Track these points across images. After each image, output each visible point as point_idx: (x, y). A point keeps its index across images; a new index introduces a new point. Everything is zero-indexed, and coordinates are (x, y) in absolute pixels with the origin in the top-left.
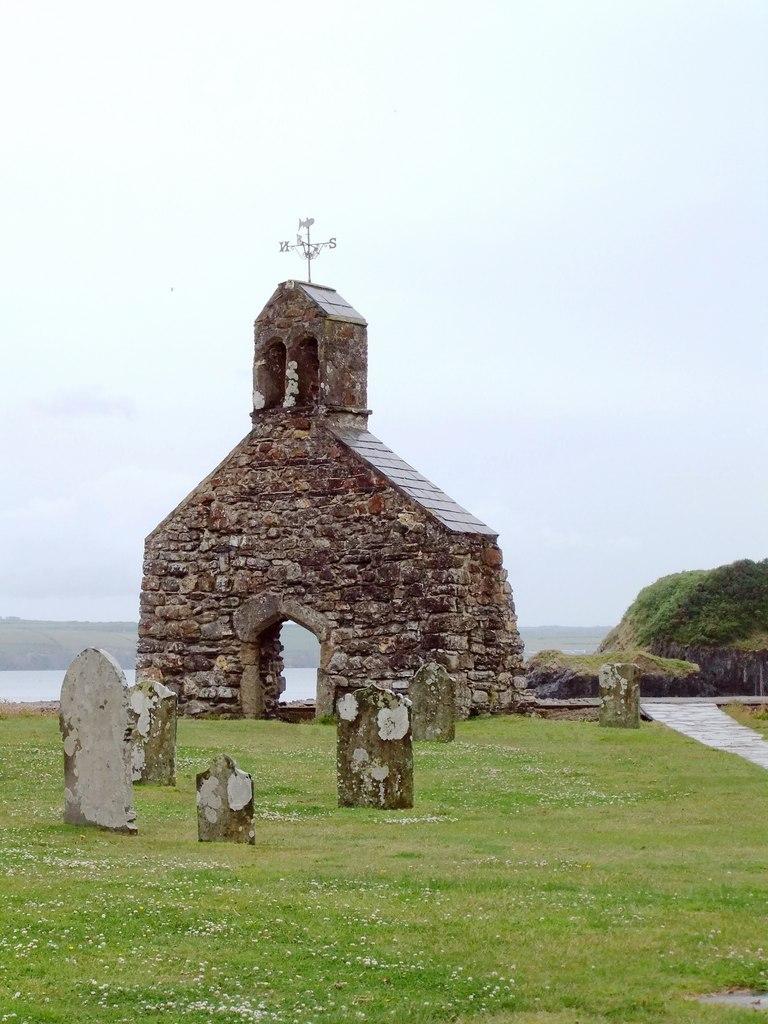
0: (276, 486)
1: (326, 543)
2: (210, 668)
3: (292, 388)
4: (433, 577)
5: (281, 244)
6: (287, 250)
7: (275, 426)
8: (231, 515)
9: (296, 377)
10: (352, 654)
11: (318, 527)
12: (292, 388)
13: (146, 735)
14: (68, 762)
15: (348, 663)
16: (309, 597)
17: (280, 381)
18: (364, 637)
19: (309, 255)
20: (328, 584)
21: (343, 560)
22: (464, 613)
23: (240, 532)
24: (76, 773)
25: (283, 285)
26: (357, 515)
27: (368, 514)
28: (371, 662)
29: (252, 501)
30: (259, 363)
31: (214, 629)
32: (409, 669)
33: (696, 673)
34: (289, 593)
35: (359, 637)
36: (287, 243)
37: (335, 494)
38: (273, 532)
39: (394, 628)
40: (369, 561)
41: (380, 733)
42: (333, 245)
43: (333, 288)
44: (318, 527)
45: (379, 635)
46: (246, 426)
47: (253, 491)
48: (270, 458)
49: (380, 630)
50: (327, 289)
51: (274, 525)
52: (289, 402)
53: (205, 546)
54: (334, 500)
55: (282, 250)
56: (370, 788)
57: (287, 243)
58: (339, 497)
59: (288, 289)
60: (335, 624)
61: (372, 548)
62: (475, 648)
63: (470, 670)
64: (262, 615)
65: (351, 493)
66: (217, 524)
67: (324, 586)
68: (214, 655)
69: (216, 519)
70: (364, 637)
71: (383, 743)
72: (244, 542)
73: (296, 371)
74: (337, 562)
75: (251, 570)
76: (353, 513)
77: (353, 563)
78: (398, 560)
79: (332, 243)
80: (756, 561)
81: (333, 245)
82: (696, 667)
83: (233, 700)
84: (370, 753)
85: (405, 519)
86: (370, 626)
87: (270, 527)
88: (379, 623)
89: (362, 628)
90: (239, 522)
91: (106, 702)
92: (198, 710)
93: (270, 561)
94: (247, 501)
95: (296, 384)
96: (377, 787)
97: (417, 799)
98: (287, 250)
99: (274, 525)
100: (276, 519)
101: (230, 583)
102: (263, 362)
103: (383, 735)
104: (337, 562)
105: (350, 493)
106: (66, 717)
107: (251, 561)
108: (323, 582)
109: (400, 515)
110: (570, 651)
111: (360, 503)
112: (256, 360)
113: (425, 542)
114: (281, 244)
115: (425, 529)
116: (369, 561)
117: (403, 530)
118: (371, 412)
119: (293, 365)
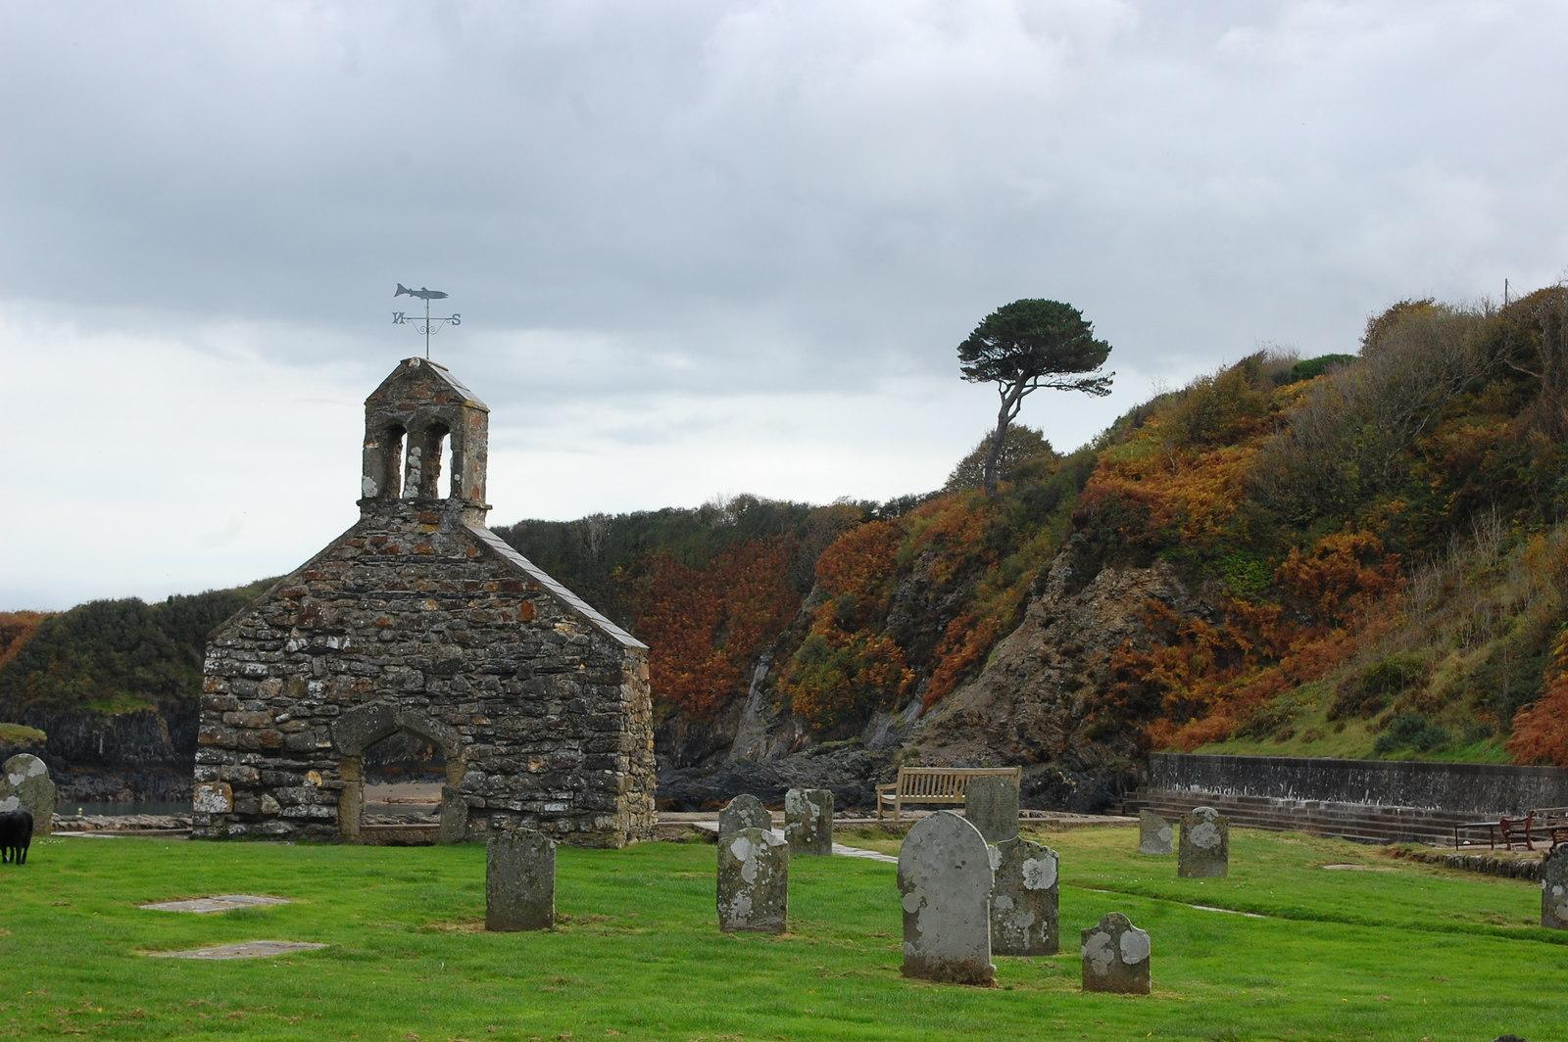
1: (457, 651)
2: (300, 783)
4: (599, 694)
5: (395, 314)
8: (327, 613)
9: (419, 464)
10: (490, 773)
11: (447, 632)
13: (752, 882)
14: (910, 919)
15: (487, 783)
16: (435, 710)
18: (508, 754)
20: (459, 696)
23: (340, 633)
24: (919, 928)
25: (405, 362)
26: (500, 622)
27: (515, 622)
28: (517, 781)
30: (371, 446)
31: (306, 740)
32: (568, 791)
33: (41, 742)
34: (408, 704)
35: (501, 755)
36: (401, 314)
38: (387, 634)
39: (547, 747)
40: (514, 672)
41: (1025, 883)
43: (446, 367)
44: (447, 632)
45: (527, 753)
46: (354, 516)
48: (385, 552)
49: (530, 748)
50: (444, 369)
51: (389, 627)
54: (471, 604)
55: (395, 322)
56: (1014, 935)
57: (401, 314)
59: (413, 366)
60: (470, 739)
61: (519, 658)
64: (372, 726)
66: (309, 623)
67: (455, 697)
68: (304, 770)
69: (308, 616)
70: (508, 754)
71: (1026, 891)
73: (420, 459)
74: (471, 671)
77: (494, 674)
78: (553, 673)
80: (116, 599)
82: (42, 734)
83: (329, 820)
84: (1015, 902)
85: (562, 628)
86: (515, 743)
87: (383, 629)
88: (524, 741)
89: (506, 745)
91: (964, 863)
92: (281, 831)
93: (382, 666)
94: (352, 598)
95: (418, 472)
96: (1022, 933)
97: (1062, 941)
98: (402, 322)
99: (389, 627)
100: (392, 621)
102: (376, 445)
103: (1027, 884)
104: (471, 671)
105: (492, 598)
106: (906, 875)
107: (357, 665)
108: (454, 693)
109: (557, 625)
112: (367, 441)
114: (395, 314)
115: (590, 641)
116: (514, 672)
117: (561, 642)
118: (491, 508)
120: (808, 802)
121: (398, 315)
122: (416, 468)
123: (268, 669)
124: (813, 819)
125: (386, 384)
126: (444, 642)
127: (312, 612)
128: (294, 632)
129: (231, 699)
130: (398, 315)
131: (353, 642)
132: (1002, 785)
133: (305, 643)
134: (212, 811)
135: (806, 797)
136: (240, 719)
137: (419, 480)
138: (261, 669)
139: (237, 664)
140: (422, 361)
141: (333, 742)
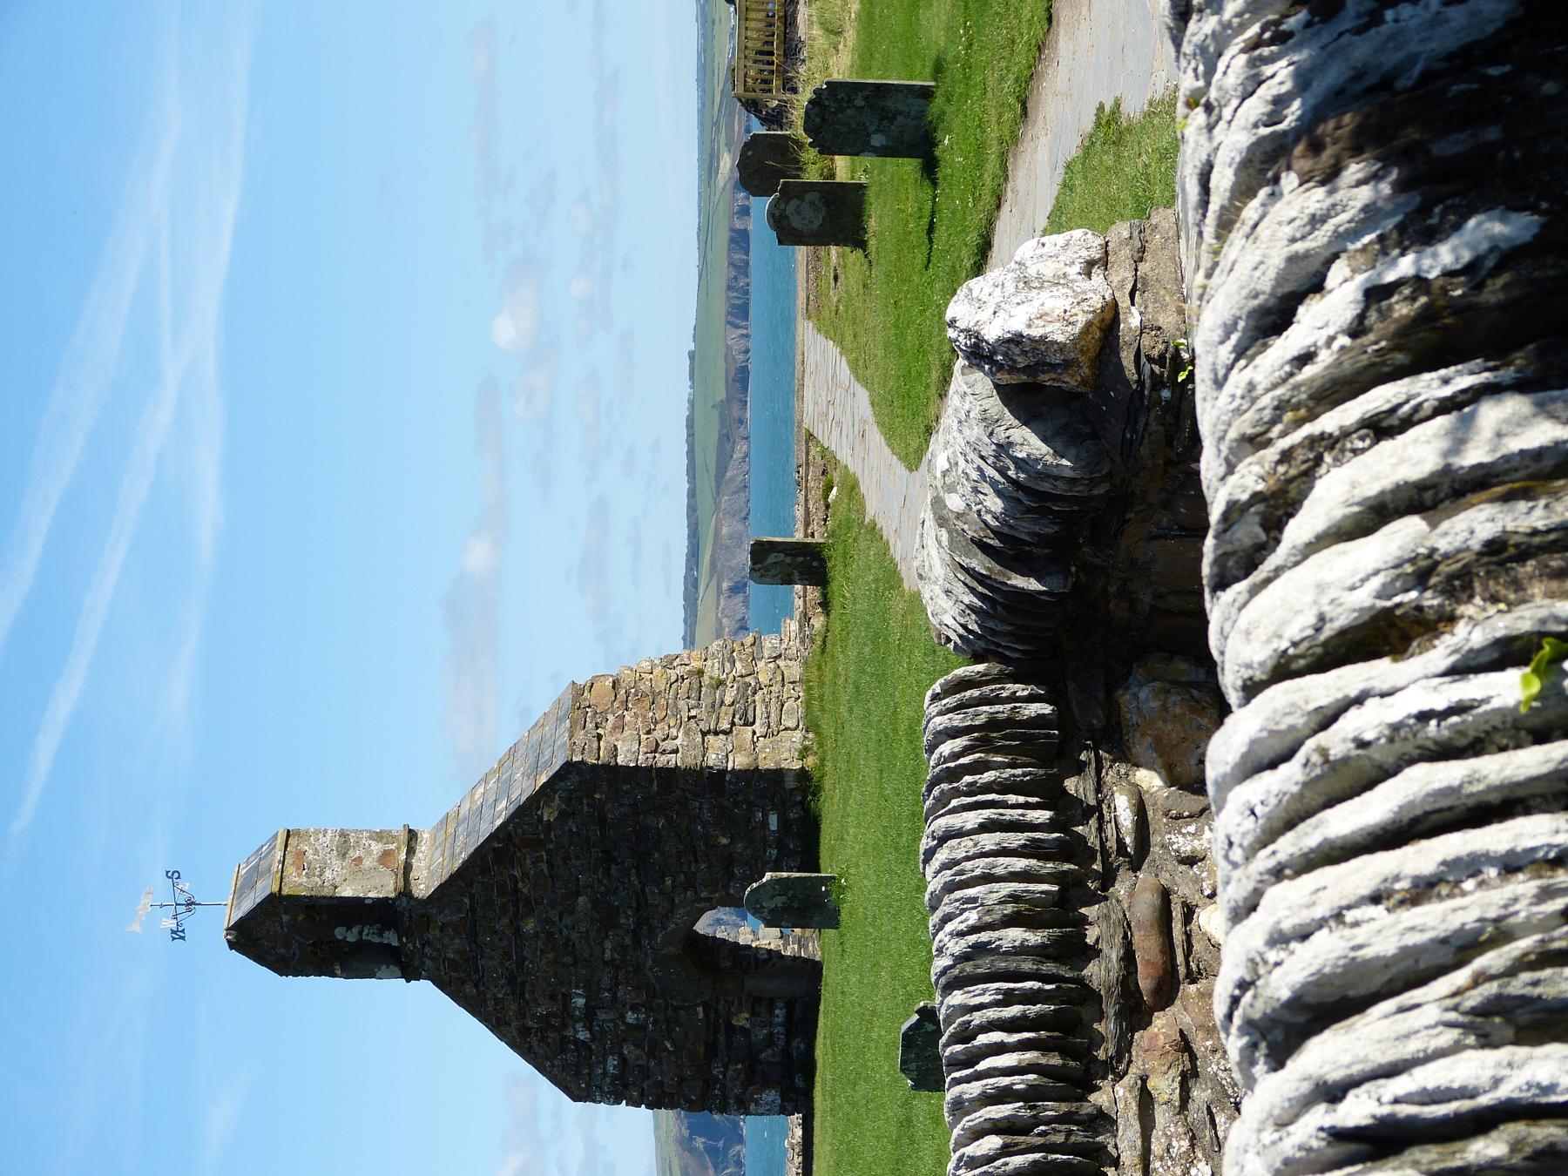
0: (507, 956)
3: (370, 935)
6: (183, 931)
7: (425, 955)
9: (355, 930)
12: (370, 935)
17: (361, 947)
19: (190, 904)
21: (605, 881)
22: (678, 742)
23: (567, 998)
26: (544, 866)
29: (524, 982)
30: (339, 972)
36: (173, 932)
37: (516, 890)
42: (176, 875)
46: (425, 987)
47: (511, 981)
52: (391, 938)
53: (583, 1035)
54: (525, 891)
55: (183, 938)
58: (520, 885)
62: (725, 725)
63: (754, 733)
65: (517, 873)
72: (580, 992)
73: (349, 928)
75: (617, 984)
76: (542, 870)
79: (174, 876)
81: (176, 875)
83: (790, 1008)
85: (548, 815)
90: (552, 997)
98: (183, 931)
101: (634, 1008)
109: (545, 818)
110: (726, 49)
111: (528, 862)
113: (564, 965)
114: (174, 939)
117: (563, 815)
119: (339, 932)
120: (766, 564)
121: (182, 934)
122: (361, 933)
123: (613, 1054)
124: (788, 560)
125: (261, 960)
126: (572, 912)
127: (545, 1020)
128: (569, 1033)
129: (648, 1086)
130: (174, 935)
131: (577, 987)
132: (669, 882)
133: (582, 1024)
134: (779, 1101)
135: (759, 566)
136: (672, 1079)
137: (374, 929)
138: (612, 1062)
139: (608, 1079)
140: (827, 83)
141: (698, 1005)
